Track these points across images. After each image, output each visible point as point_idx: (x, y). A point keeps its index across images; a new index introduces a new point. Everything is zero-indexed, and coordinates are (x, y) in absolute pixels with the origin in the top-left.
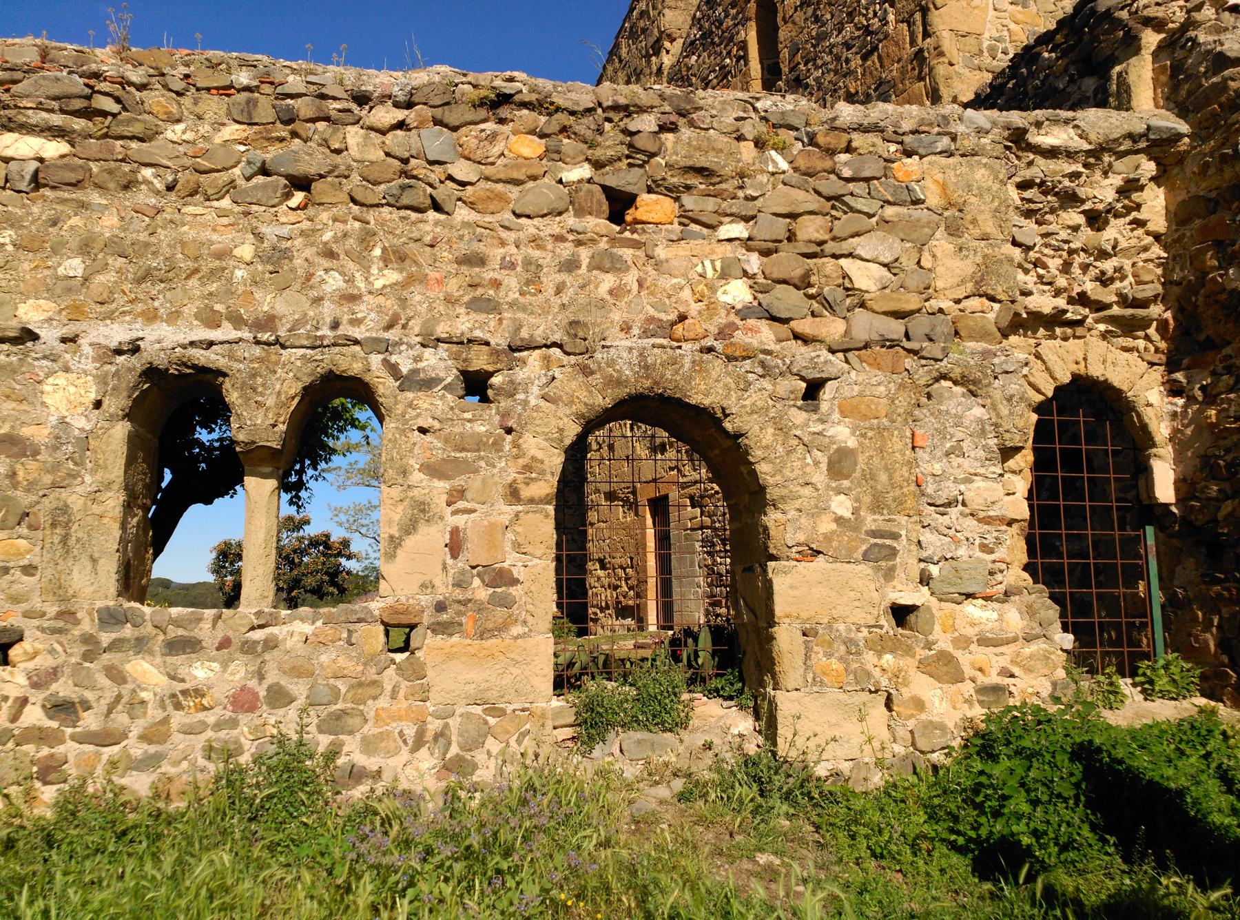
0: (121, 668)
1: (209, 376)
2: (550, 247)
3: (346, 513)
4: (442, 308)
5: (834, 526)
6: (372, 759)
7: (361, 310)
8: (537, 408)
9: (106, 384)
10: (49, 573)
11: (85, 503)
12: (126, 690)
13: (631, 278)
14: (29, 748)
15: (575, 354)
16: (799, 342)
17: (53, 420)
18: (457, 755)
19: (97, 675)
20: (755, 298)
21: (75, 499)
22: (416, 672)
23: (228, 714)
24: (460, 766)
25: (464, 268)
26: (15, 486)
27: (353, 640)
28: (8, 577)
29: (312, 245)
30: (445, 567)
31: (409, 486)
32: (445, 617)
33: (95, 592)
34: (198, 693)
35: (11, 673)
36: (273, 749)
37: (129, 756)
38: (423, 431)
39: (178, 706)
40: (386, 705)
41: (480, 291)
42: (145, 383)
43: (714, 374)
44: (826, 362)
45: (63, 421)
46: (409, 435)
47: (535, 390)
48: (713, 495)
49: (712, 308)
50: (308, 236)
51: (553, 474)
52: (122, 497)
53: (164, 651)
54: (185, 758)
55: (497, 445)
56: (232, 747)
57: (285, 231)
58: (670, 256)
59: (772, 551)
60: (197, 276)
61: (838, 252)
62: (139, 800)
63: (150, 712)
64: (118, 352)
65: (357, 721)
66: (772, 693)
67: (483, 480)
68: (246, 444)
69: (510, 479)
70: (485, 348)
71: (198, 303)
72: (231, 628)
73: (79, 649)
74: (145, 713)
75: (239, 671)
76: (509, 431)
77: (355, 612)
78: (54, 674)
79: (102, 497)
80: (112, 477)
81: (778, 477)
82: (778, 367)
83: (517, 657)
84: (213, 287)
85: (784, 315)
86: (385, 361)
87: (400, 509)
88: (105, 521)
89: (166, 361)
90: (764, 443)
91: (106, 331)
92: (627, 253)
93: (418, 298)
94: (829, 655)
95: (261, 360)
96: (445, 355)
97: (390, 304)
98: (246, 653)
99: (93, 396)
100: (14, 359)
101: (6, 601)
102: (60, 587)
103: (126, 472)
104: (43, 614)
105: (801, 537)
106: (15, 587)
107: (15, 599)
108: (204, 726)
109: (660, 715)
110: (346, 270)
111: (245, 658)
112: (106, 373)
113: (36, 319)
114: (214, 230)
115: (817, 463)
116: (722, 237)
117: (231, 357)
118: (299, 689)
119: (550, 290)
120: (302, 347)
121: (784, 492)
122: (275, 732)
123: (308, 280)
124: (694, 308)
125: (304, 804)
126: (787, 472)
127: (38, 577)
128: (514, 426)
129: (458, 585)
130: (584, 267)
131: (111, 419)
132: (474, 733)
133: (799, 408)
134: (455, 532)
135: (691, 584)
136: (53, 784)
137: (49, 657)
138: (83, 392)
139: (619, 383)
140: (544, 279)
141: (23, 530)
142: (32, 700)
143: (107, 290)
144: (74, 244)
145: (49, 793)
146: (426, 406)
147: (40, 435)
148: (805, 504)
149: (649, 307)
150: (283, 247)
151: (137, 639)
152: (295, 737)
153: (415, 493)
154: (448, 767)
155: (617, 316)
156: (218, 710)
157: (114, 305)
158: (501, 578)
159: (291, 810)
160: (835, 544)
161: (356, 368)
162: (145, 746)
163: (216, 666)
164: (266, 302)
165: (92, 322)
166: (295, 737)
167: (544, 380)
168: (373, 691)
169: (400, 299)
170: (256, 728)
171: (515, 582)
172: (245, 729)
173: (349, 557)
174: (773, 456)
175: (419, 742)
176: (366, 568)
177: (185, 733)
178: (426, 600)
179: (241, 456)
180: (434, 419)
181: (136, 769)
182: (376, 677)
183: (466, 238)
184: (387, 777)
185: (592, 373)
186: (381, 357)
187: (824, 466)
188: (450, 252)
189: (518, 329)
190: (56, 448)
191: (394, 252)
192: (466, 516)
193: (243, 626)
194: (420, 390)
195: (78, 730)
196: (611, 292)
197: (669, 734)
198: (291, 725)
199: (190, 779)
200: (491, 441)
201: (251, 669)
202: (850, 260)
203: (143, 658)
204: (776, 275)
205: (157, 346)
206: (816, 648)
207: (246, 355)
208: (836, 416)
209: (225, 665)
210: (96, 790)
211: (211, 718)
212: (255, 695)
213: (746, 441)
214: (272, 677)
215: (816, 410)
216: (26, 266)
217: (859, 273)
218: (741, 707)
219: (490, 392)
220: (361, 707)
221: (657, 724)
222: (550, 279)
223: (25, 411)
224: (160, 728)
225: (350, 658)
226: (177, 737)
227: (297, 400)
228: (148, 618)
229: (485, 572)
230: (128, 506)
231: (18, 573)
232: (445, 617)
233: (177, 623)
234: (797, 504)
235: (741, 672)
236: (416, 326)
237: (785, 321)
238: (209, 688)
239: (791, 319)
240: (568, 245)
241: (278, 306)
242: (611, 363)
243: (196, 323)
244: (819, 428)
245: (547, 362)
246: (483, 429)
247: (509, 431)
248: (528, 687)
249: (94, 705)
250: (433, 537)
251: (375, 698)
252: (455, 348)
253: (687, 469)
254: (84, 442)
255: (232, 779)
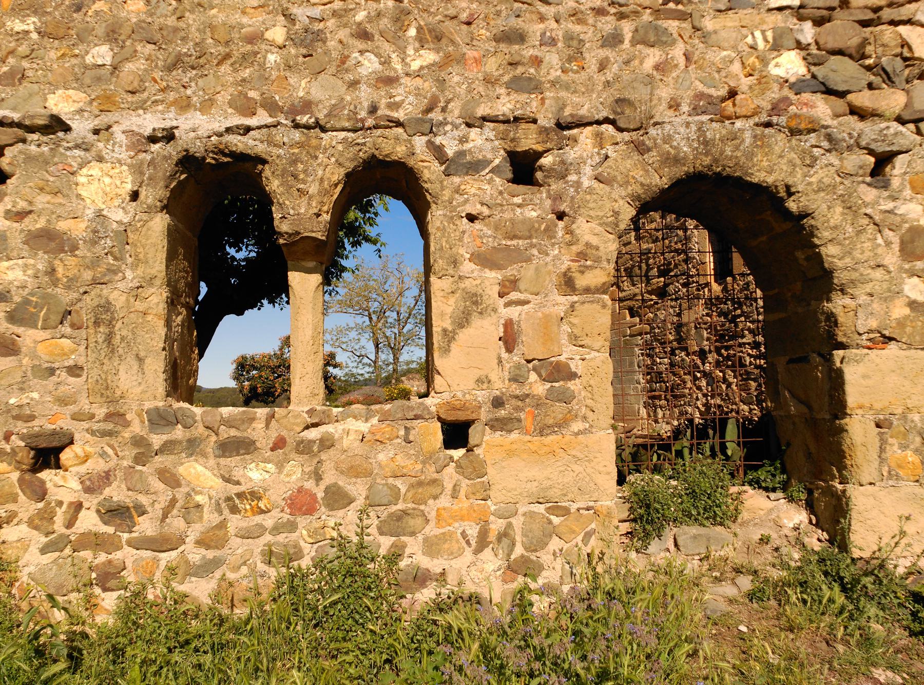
0: (174, 471)
1: (248, 165)
2: (591, 21)
3: (330, 334)
4: (481, 89)
5: (907, 311)
6: (435, 561)
7: (399, 94)
8: (590, 191)
9: (142, 173)
10: (95, 373)
11: (128, 300)
12: (180, 493)
13: (678, 52)
14: (87, 554)
15: (628, 130)
16: (856, 117)
17: (90, 213)
18: (522, 556)
19: (150, 478)
20: (809, 71)
21: (117, 296)
22: (475, 470)
23: (286, 517)
24: (526, 568)
25: (503, 46)
26: (55, 283)
27: (411, 438)
28: (54, 379)
29: (345, 26)
30: (500, 361)
31: (460, 277)
32: (502, 413)
33: (143, 392)
34: (255, 496)
35: (63, 477)
36: (333, 552)
37: (187, 562)
38: (471, 218)
39: (234, 510)
40: (448, 505)
41: (520, 70)
42: (182, 173)
43: (777, 150)
44: (896, 134)
45: (99, 214)
46: (458, 222)
47: (588, 170)
48: (652, 306)
49: (763, 81)
50: (340, 17)
51: (608, 261)
52: (165, 294)
53: (217, 452)
54: (244, 563)
55: (549, 232)
56: (292, 551)
57: (316, 12)
58: (717, 27)
59: (841, 339)
60: (229, 62)
61: (897, 19)
62: (199, 608)
63: (206, 516)
64: (153, 139)
65: (419, 521)
66: (840, 487)
67: (537, 269)
68: (290, 235)
69: (564, 268)
70: (532, 126)
71: (231, 90)
72: (286, 428)
73: (130, 453)
74: (201, 518)
75: (295, 473)
76: (561, 216)
77: (411, 408)
78: (106, 477)
79: (144, 293)
80: (153, 272)
81: (848, 260)
82: (845, 140)
83: (579, 454)
84: (246, 73)
85: (841, 88)
86: (430, 143)
87: (452, 301)
88: (149, 318)
89: (202, 149)
90: (832, 223)
91: (139, 121)
92: (673, 25)
93: (456, 79)
94: (904, 447)
95: (301, 145)
96: (492, 135)
97: (428, 86)
98: (302, 453)
99: (129, 187)
100: (45, 149)
101: (53, 403)
102: (107, 388)
103: (167, 267)
104: (92, 416)
105: (873, 324)
106: (62, 388)
107: (63, 401)
108: (261, 530)
109: (710, 510)
110: (382, 51)
111: (301, 458)
112: (142, 163)
113: (66, 110)
114: (244, 13)
115: (888, 244)
116: (773, 5)
117: (270, 142)
118: (358, 489)
119: (593, 66)
120: (343, 130)
121: (855, 275)
122: (335, 534)
123: (343, 63)
124: (745, 83)
125: (369, 609)
126: (857, 254)
127: (84, 377)
128: (567, 210)
129: (514, 379)
130: (627, 42)
131: (149, 210)
132: (538, 533)
133: (869, 185)
134: (508, 325)
135: (631, 381)
136: (113, 590)
137: (100, 460)
138: (118, 183)
139: (677, 160)
140: (586, 55)
141: (66, 329)
142: (86, 505)
143: (137, 79)
144: (100, 30)
145: (109, 600)
146: (473, 191)
147: (78, 229)
148: (877, 288)
149: (697, 83)
150: (316, 28)
151: (189, 441)
152: (355, 539)
153: (467, 284)
154: (512, 569)
155: (664, 93)
156: (275, 513)
157: (146, 94)
158: (559, 372)
159: (357, 617)
160: (908, 330)
161: (399, 152)
162: (203, 551)
163: (270, 466)
164: (302, 87)
165: (124, 113)
166: (355, 539)
167: (597, 159)
168: (434, 490)
169: (437, 80)
170: (316, 531)
171: (573, 376)
172: (304, 532)
173: (335, 366)
174: (841, 237)
175: (482, 543)
176: (347, 374)
177: (243, 537)
178: (482, 395)
179: (284, 249)
180: (482, 204)
181: (195, 575)
182: (435, 476)
183: (504, 14)
184: (452, 579)
185: (649, 150)
186: (425, 139)
187: (896, 247)
188: (487, 30)
189: (562, 108)
190: (94, 243)
191: (430, 31)
192: (519, 308)
193: (298, 425)
194: (467, 174)
195: (134, 535)
196: (657, 67)
197: (719, 529)
198: (350, 527)
199: (251, 585)
200: (543, 227)
201: (307, 470)
202: (908, 27)
203: (196, 460)
204: (832, 44)
205: (192, 134)
206: (890, 440)
207: (286, 140)
208: (908, 193)
209: (280, 466)
210: (156, 596)
211: (269, 521)
212: (313, 497)
213: (812, 222)
214: (330, 477)
215: (886, 186)
216: (53, 54)
217: (919, 41)
218: (791, 499)
219: (539, 175)
220: (422, 507)
221: (707, 518)
222: (592, 56)
223: (60, 204)
224: (217, 532)
225: (409, 456)
226: (235, 542)
227: (339, 188)
228: (198, 418)
229: (542, 367)
230: (172, 304)
231: (64, 374)
232: (502, 413)
233: (229, 423)
234: (868, 288)
235: (782, 464)
236: (455, 108)
237: (842, 95)
238: (265, 490)
239: (849, 92)
240: (609, 18)
241: (313, 91)
242: (668, 139)
243: (230, 111)
244: (890, 205)
245: (599, 139)
246: (534, 214)
247: (561, 216)
248: (592, 485)
249: (149, 509)
250: (486, 330)
251: (435, 498)
252: (502, 127)
253: (626, 285)
254: (124, 234)
255: (293, 583)
